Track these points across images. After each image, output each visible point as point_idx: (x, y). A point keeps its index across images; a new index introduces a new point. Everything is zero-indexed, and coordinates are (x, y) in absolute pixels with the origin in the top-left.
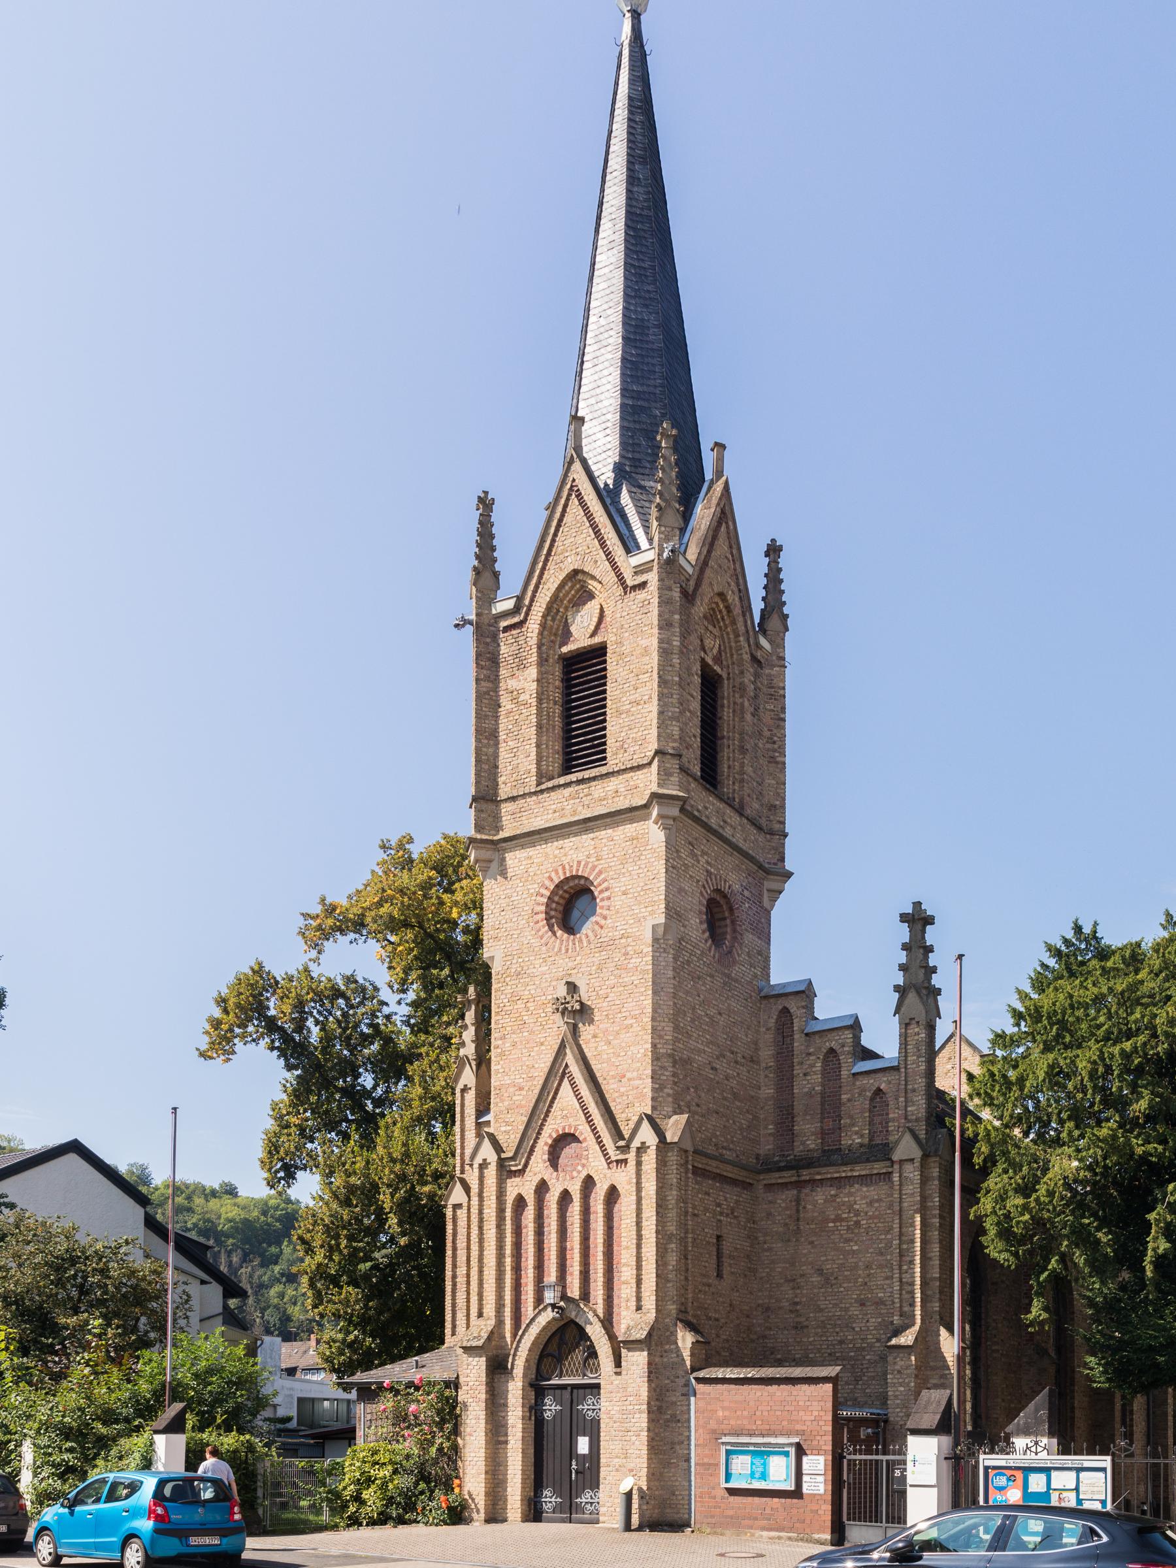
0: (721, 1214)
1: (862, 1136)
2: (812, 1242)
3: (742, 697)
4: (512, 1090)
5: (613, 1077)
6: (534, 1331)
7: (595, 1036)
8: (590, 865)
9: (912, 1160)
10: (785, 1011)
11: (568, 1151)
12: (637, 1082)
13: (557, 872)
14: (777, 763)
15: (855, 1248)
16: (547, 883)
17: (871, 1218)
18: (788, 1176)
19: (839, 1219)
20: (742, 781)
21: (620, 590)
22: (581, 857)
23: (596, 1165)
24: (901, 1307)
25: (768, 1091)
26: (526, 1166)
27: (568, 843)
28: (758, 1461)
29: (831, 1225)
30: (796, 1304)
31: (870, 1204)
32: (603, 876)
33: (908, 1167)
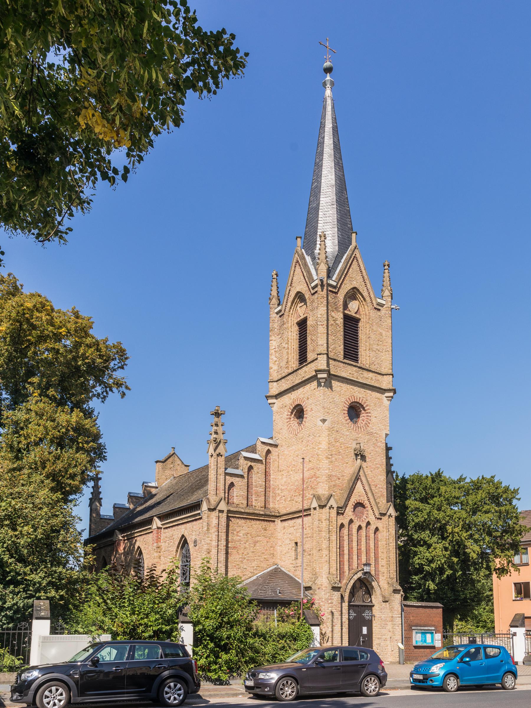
11: (360, 509)
12: (381, 490)
18: (338, 547)
27: (356, 389)
28: (423, 636)
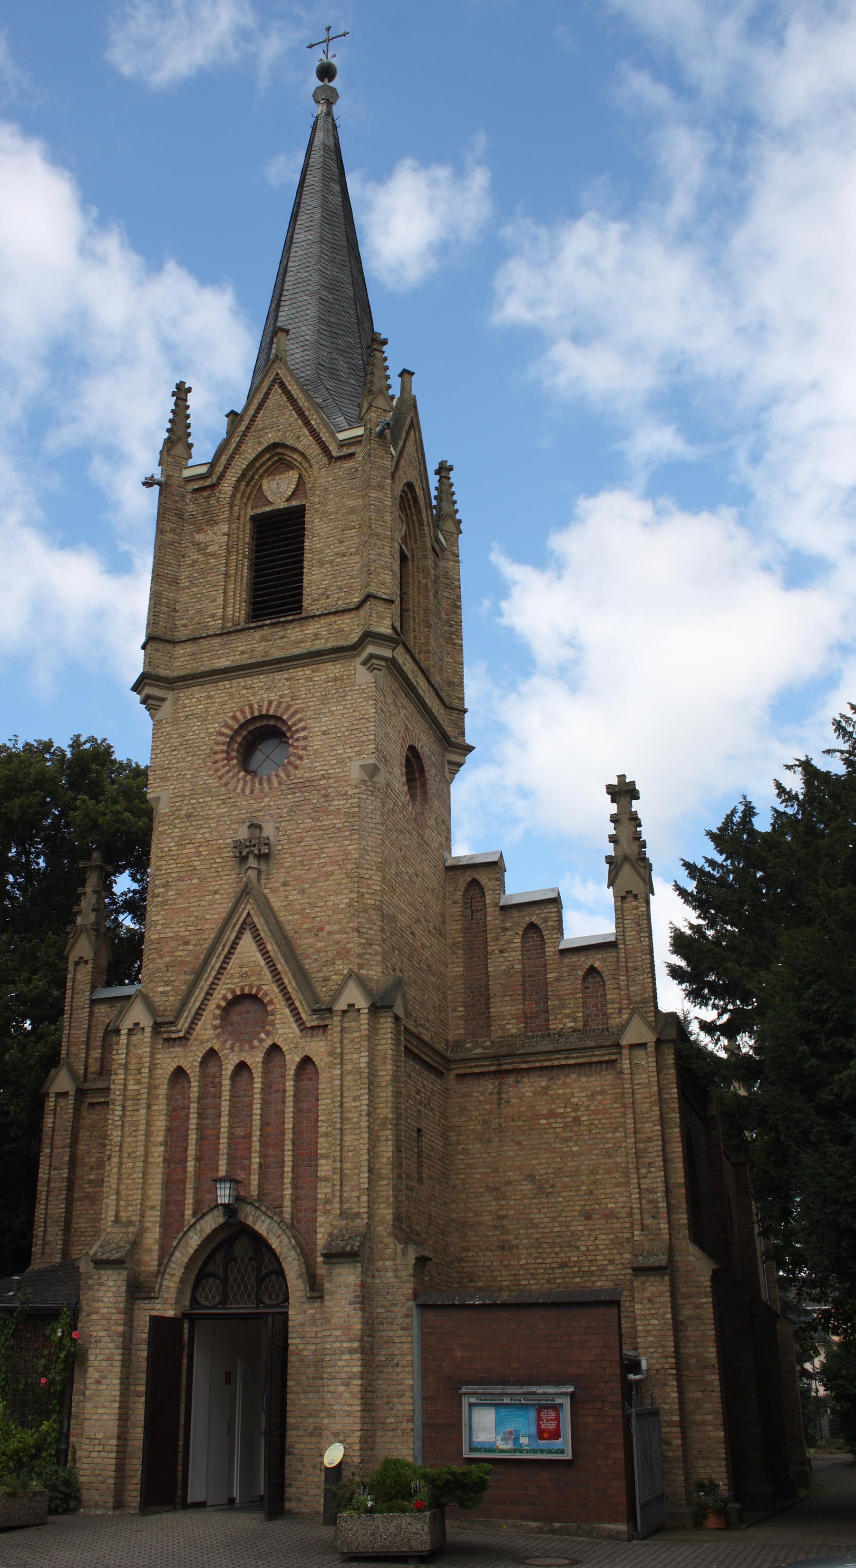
0: (420, 1103)
1: (575, 1020)
2: (520, 1143)
3: (425, 578)
4: (174, 944)
5: (309, 930)
6: (194, 1241)
7: (285, 884)
8: (284, 705)
9: (644, 1045)
10: (475, 883)
12: (338, 937)
13: (242, 711)
14: (454, 644)
15: (576, 1149)
16: (230, 722)
17: (594, 1113)
19: (552, 1114)
20: (428, 652)
21: (325, 460)
22: (273, 696)
23: (285, 1030)
24: (642, 1219)
25: (456, 969)
26: (191, 1028)
29: (543, 1121)
30: (503, 1217)
31: (592, 1096)
32: (298, 716)
33: (639, 1053)
